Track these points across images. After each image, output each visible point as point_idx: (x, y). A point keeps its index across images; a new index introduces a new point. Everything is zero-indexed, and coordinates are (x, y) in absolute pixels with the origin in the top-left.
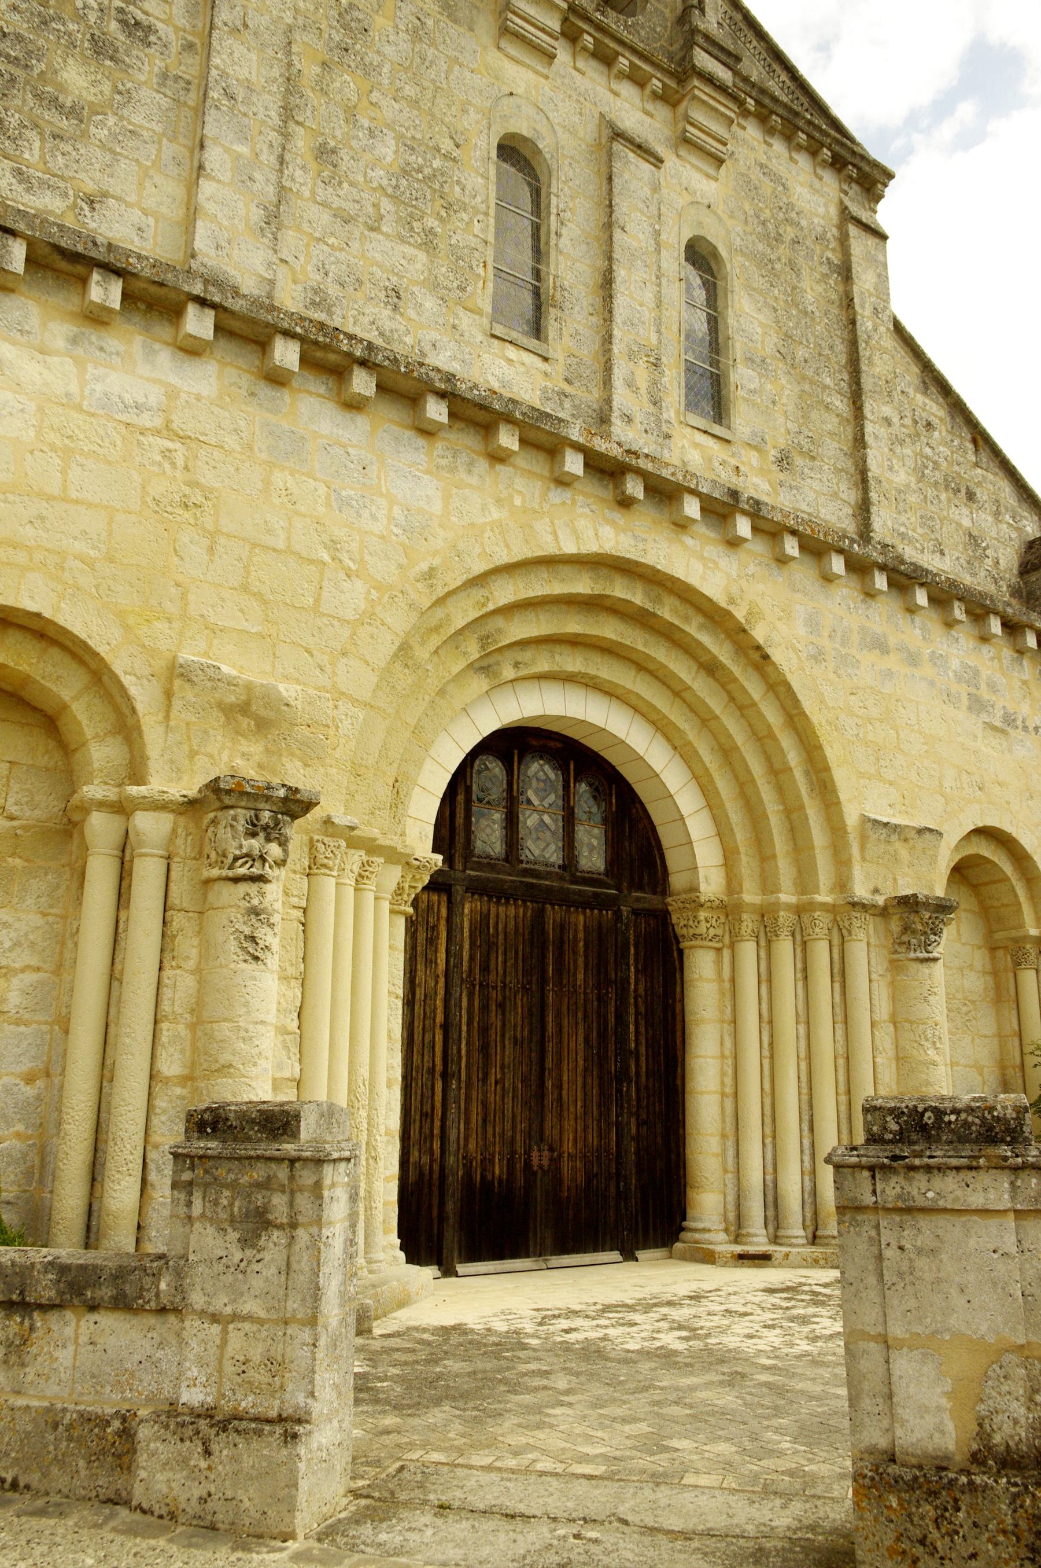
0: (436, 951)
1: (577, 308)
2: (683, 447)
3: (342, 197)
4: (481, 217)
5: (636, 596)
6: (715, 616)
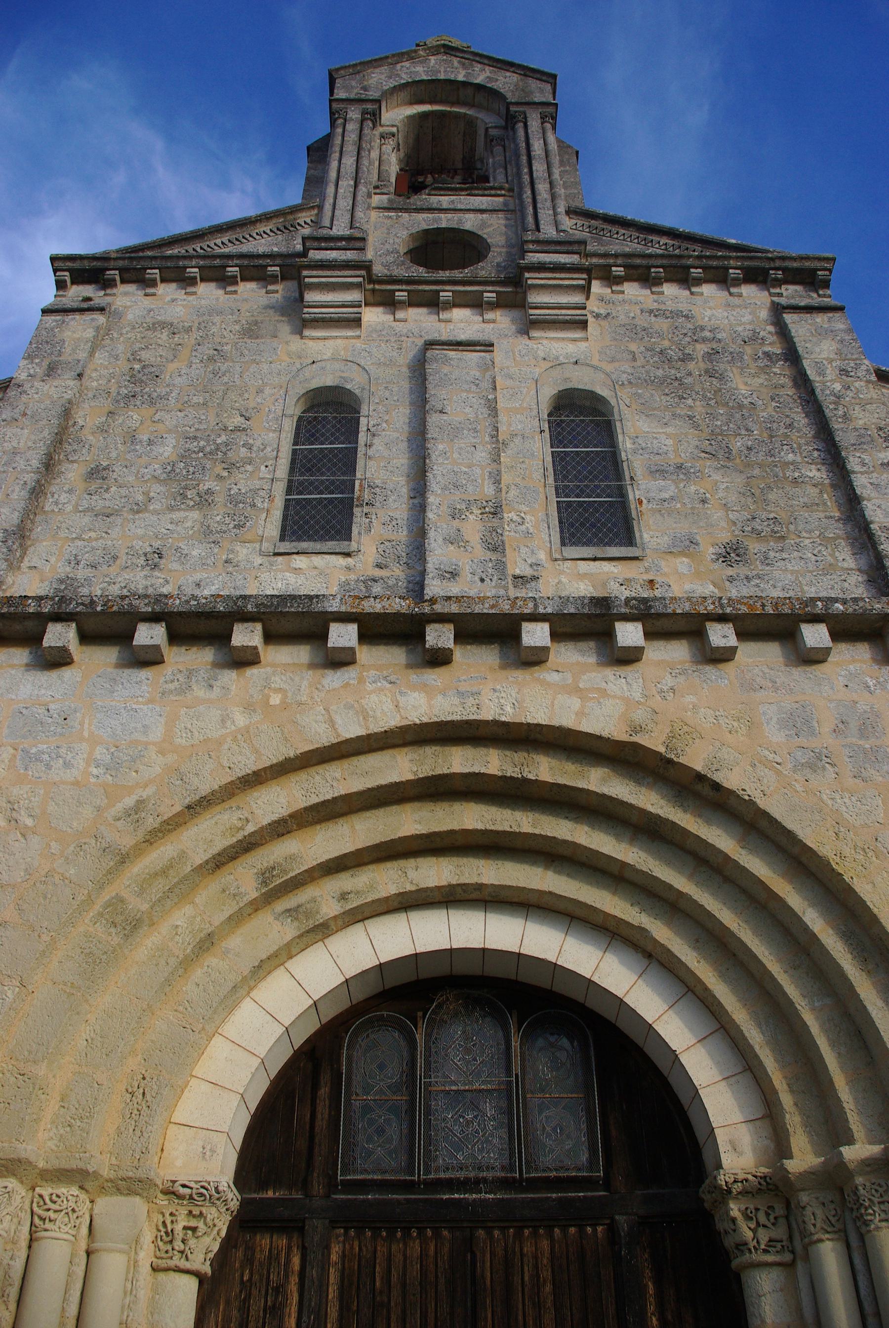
5: (492, 762)
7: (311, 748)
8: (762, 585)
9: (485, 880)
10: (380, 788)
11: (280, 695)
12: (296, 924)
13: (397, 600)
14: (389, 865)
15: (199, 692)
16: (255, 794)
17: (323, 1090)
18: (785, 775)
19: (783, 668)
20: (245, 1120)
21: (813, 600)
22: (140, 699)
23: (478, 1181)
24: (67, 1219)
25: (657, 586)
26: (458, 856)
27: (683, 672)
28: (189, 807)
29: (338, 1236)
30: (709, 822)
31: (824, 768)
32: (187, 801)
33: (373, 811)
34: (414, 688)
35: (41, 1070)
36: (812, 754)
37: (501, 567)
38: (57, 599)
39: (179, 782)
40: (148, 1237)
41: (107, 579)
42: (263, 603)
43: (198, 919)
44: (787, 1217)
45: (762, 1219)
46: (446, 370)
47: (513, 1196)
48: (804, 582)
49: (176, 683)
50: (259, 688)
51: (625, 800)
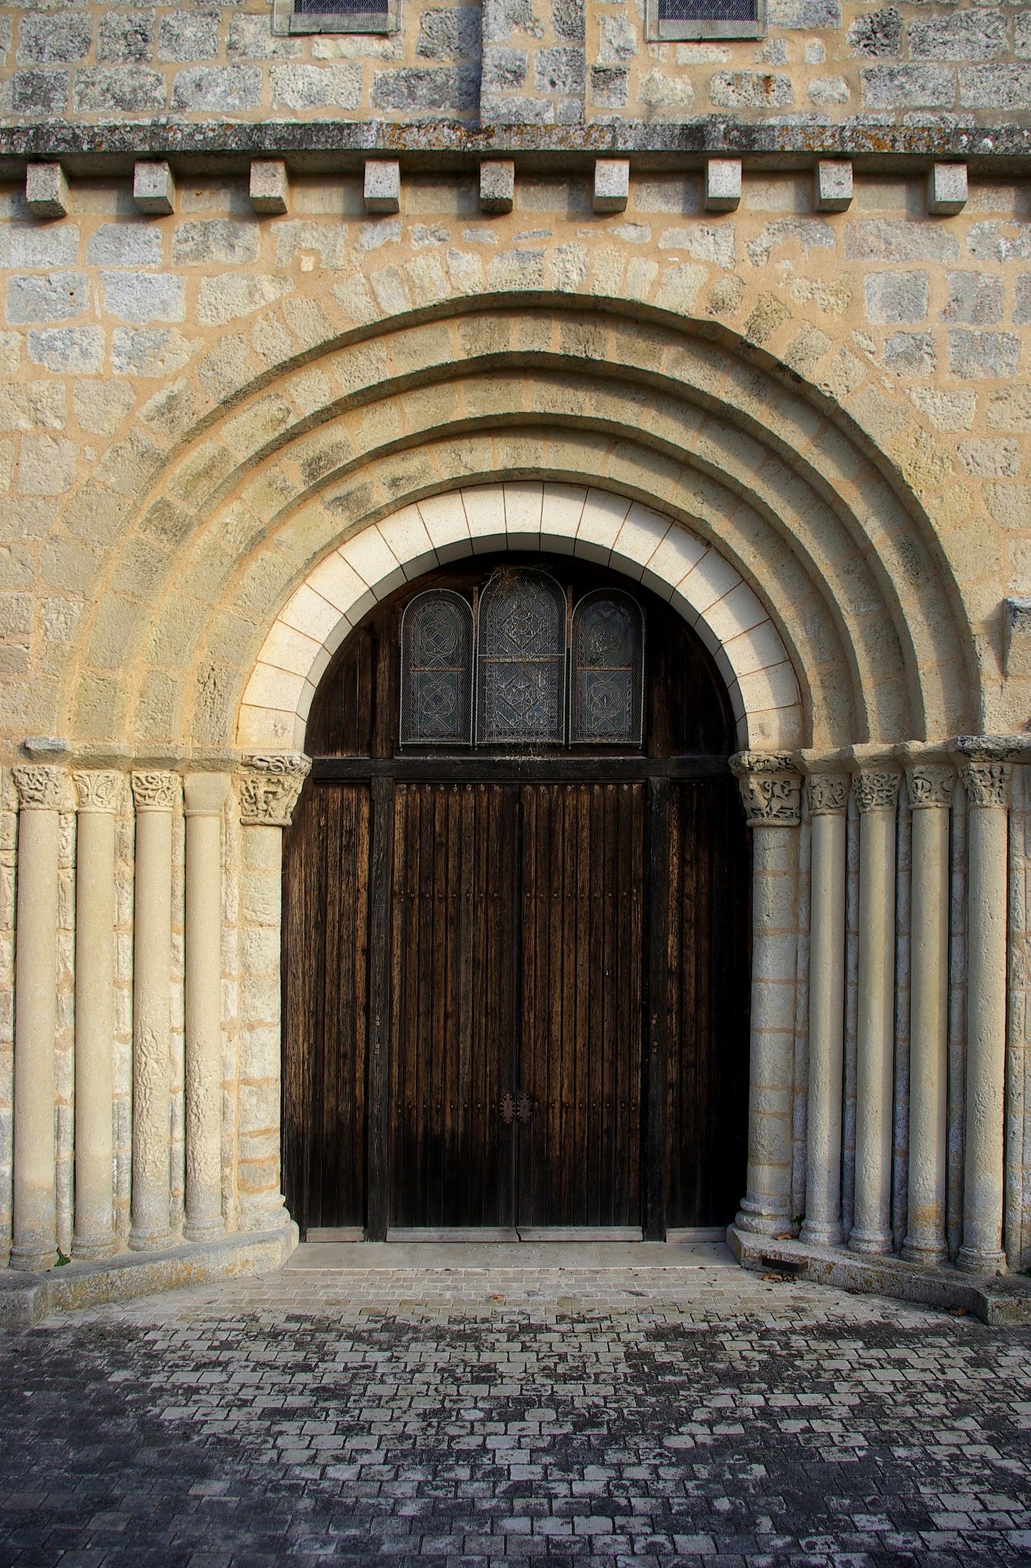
0: (355, 862)
5: (553, 338)
6: (704, 338)
7: (352, 328)
8: (907, 86)
9: (543, 465)
10: (430, 369)
11: (313, 259)
12: (347, 513)
13: (446, 131)
14: (442, 446)
15: (219, 255)
16: (294, 379)
17: (382, 664)
18: (876, 369)
19: (903, 223)
20: (311, 693)
21: (958, 132)
22: (153, 266)
23: (527, 745)
24: (163, 796)
25: (774, 86)
26: (515, 436)
27: (784, 228)
28: (225, 402)
29: (401, 790)
30: (784, 415)
31: (921, 360)
32: (222, 397)
33: (424, 391)
34: (466, 247)
35: (119, 675)
36: (912, 341)
37: (576, 61)
38: (31, 132)
39: (211, 373)
40: (234, 800)
41: (83, 78)
42: (283, 137)
43: (247, 516)
44: (800, 790)
45: (777, 790)
47: (560, 758)
48: (963, 82)
49: (191, 243)
50: (287, 249)
51: (697, 386)
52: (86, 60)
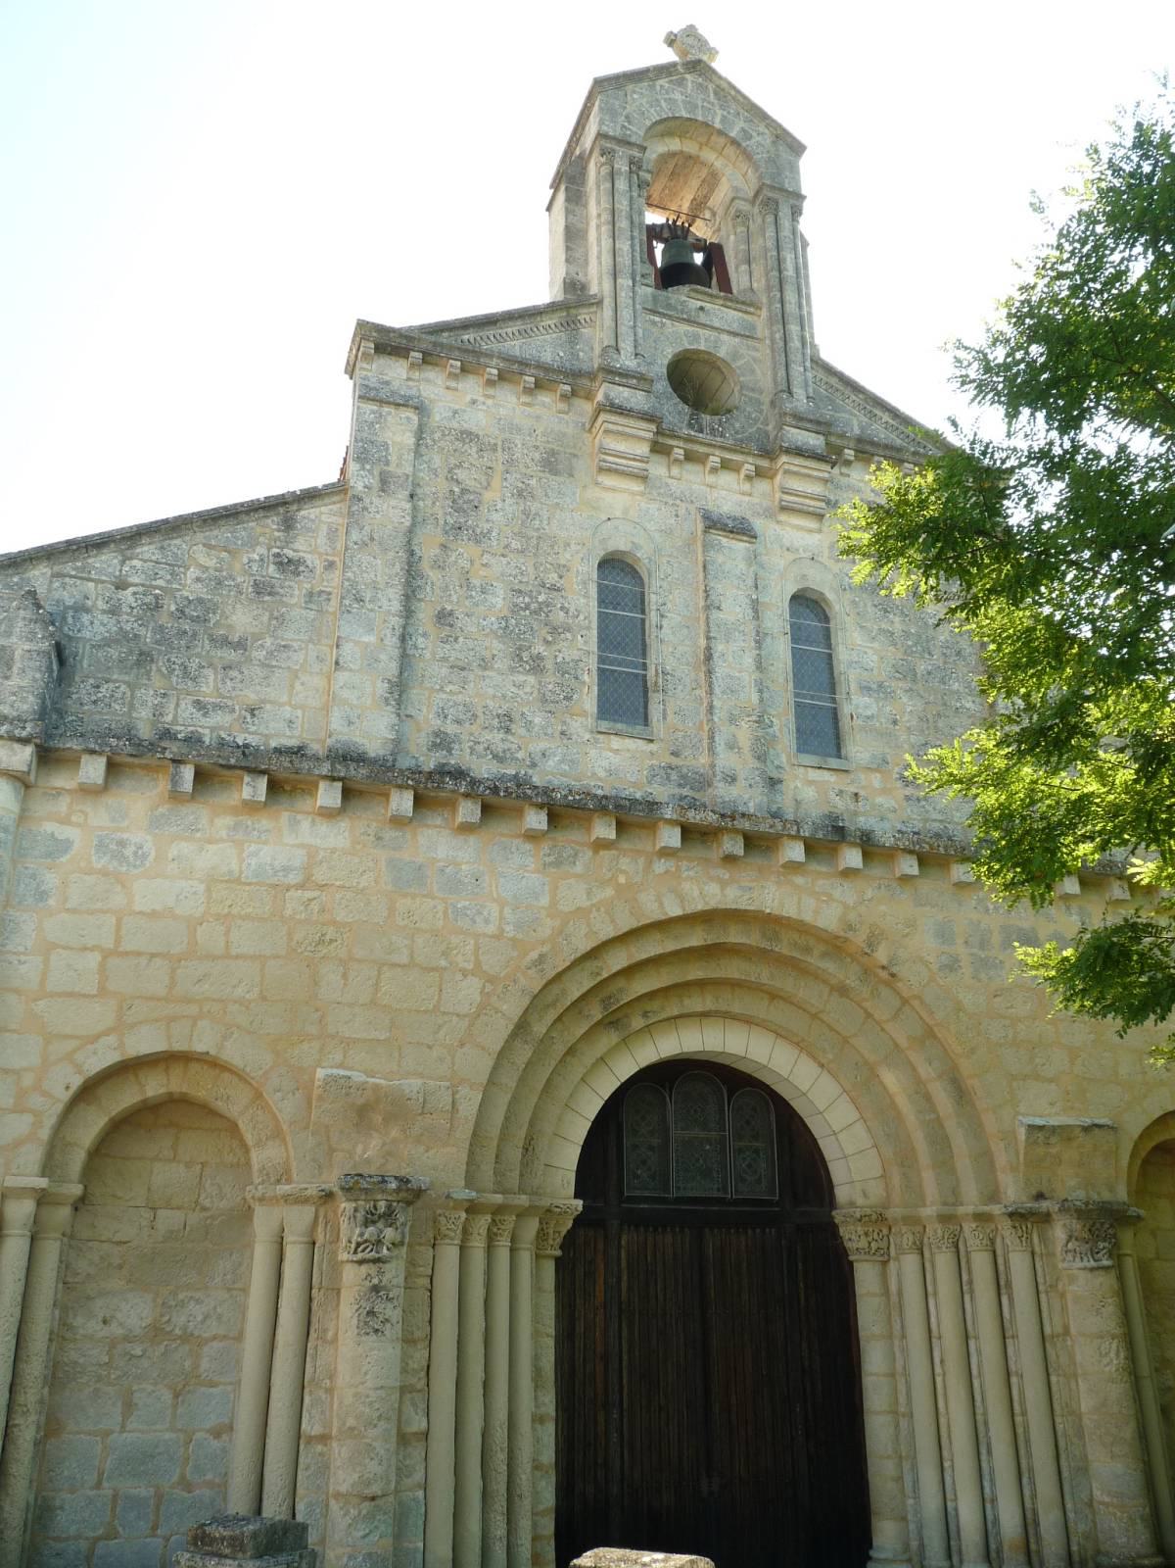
1: (680, 687)
2: (796, 787)
3: (455, 652)
4: (584, 632)
46: (720, 559)
52: (474, 727)
